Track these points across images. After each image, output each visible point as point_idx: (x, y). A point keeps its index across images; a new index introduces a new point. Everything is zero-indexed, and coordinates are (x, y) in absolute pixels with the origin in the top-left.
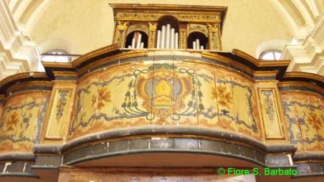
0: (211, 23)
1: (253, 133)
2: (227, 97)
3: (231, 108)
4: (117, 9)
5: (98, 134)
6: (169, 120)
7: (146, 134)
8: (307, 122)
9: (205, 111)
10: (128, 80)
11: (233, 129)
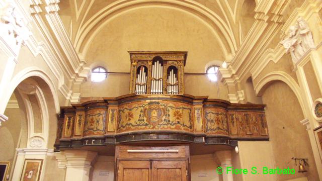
0: (180, 61)
1: (190, 130)
2: (180, 115)
3: (181, 120)
4: (131, 54)
5: (130, 132)
6: (156, 127)
7: (148, 133)
8: (214, 121)
9: (171, 123)
10: (140, 109)
11: (181, 129)
